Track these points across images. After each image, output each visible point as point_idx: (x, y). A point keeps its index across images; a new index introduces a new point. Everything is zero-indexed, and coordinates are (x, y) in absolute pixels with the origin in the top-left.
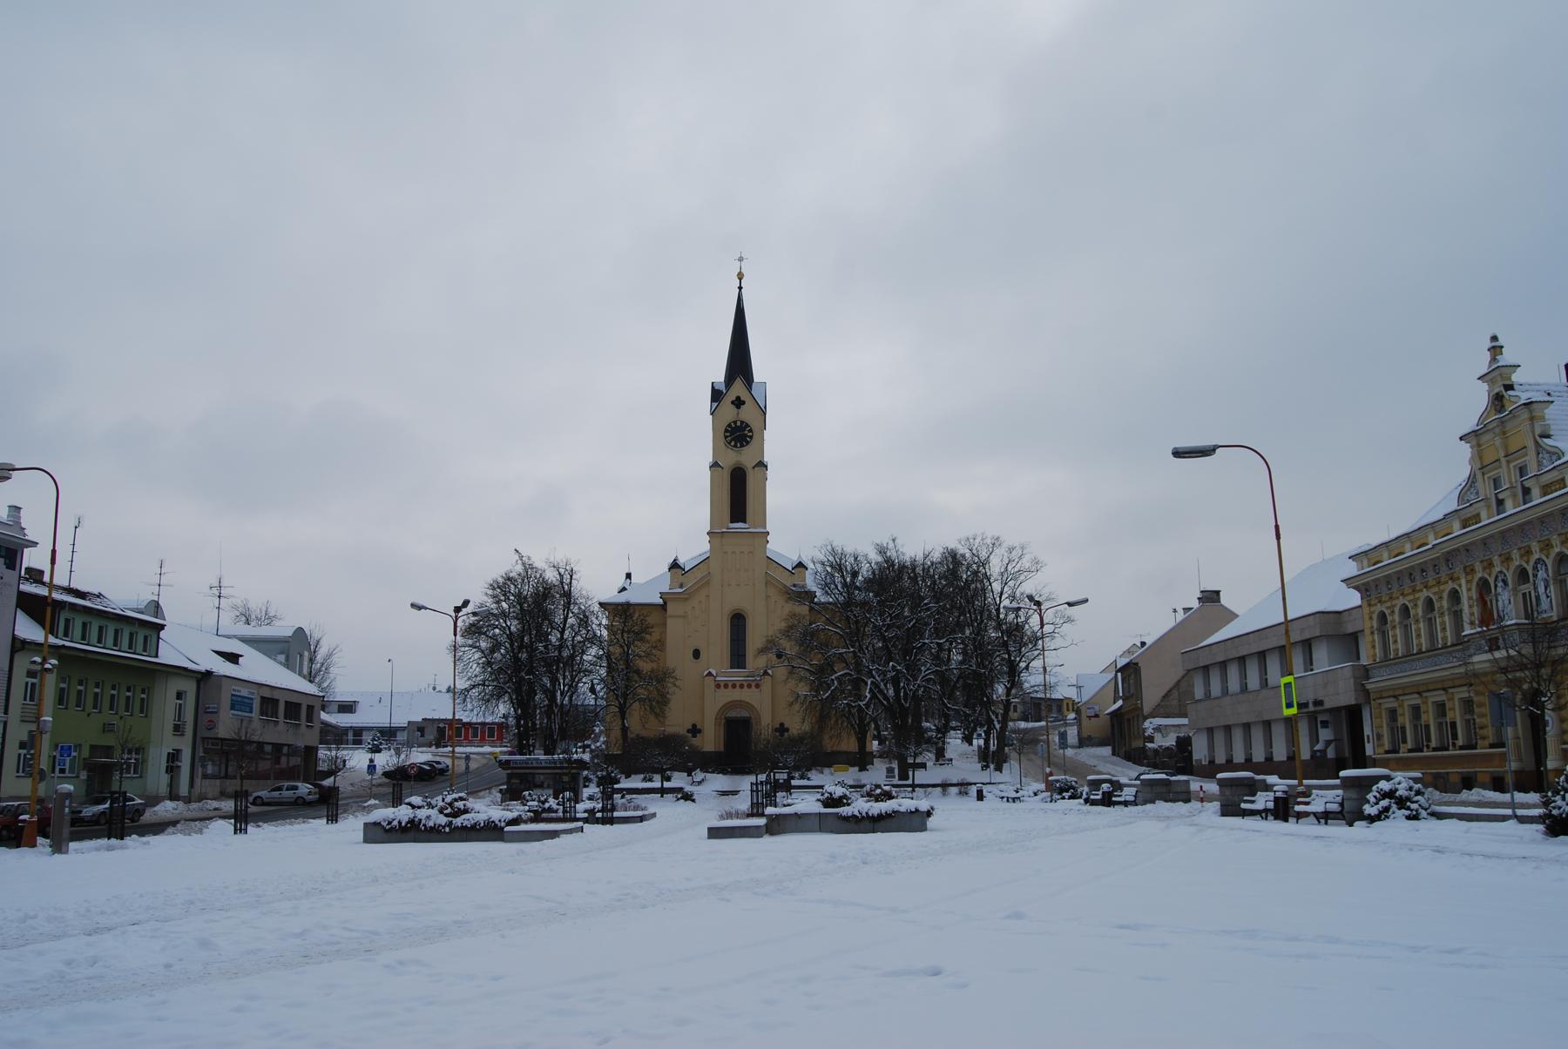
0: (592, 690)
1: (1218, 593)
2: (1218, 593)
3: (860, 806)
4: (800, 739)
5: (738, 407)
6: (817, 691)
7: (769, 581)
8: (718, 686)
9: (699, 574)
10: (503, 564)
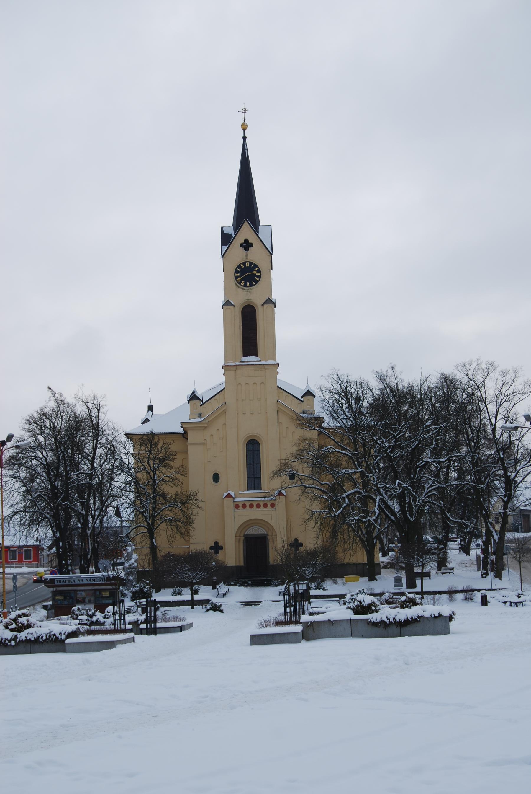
0: (118, 513)
3: (386, 613)
4: (314, 554)
5: (247, 249)
6: (330, 509)
7: (280, 409)
8: (237, 507)
9: (216, 404)
10: (38, 401)
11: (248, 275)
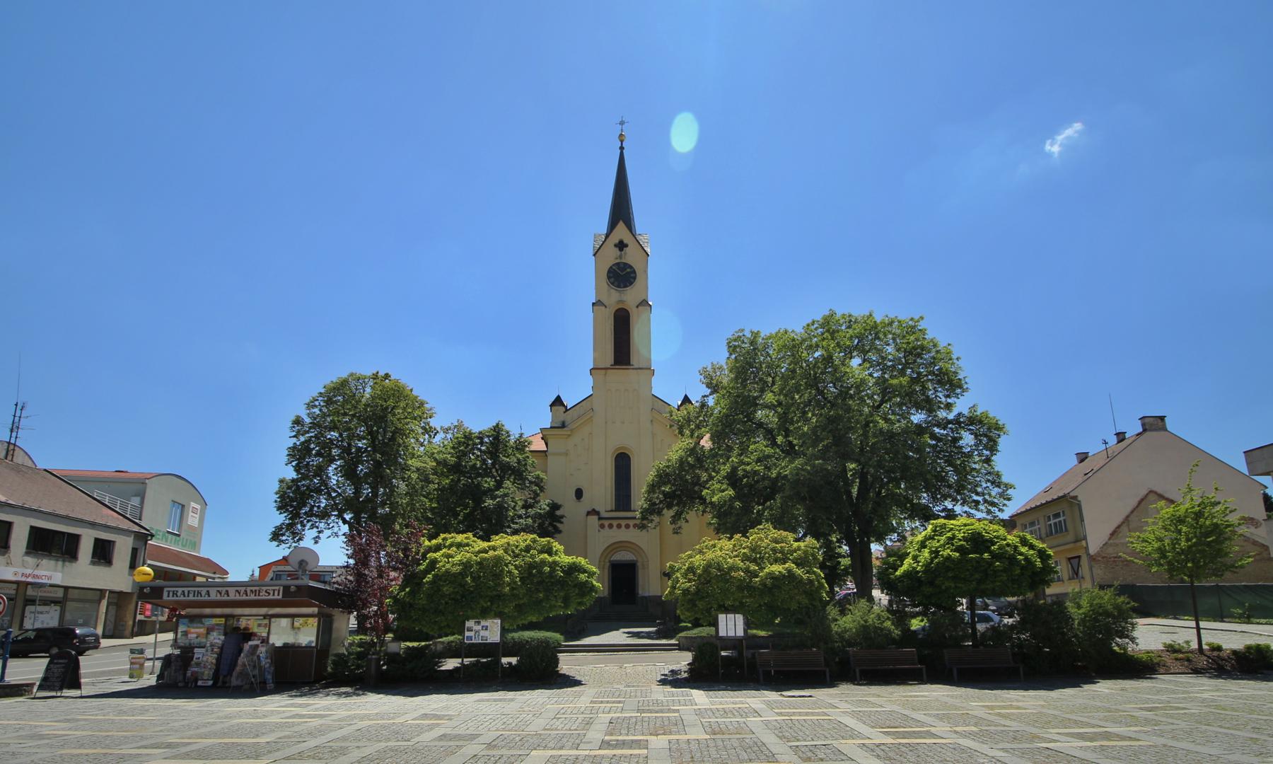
1: (1162, 418)
2: (1162, 418)
5: (621, 250)
8: (602, 526)
11: (622, 275)
